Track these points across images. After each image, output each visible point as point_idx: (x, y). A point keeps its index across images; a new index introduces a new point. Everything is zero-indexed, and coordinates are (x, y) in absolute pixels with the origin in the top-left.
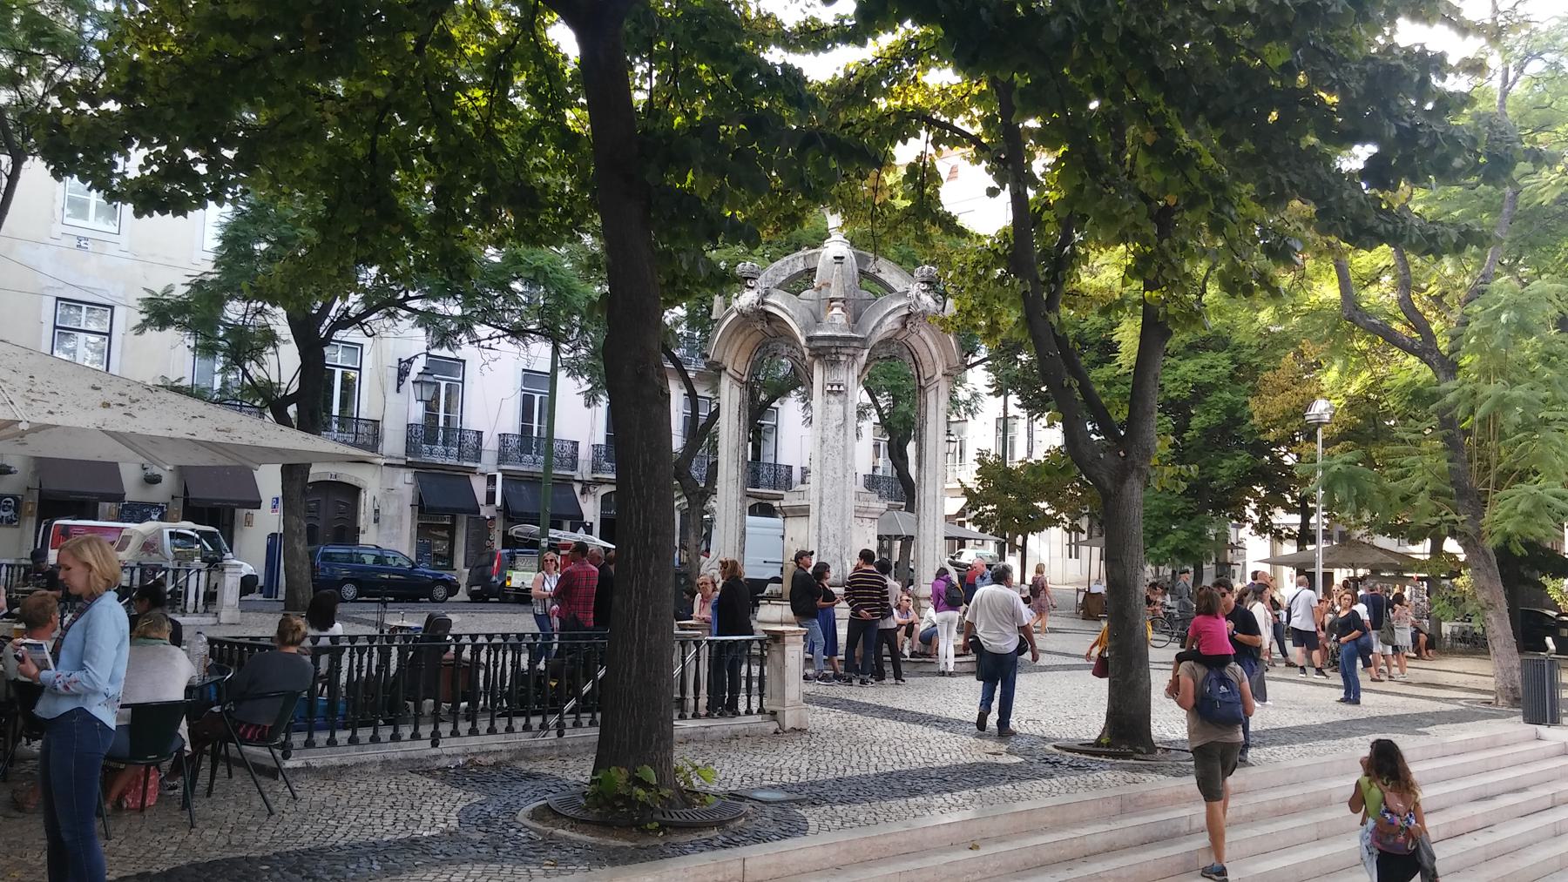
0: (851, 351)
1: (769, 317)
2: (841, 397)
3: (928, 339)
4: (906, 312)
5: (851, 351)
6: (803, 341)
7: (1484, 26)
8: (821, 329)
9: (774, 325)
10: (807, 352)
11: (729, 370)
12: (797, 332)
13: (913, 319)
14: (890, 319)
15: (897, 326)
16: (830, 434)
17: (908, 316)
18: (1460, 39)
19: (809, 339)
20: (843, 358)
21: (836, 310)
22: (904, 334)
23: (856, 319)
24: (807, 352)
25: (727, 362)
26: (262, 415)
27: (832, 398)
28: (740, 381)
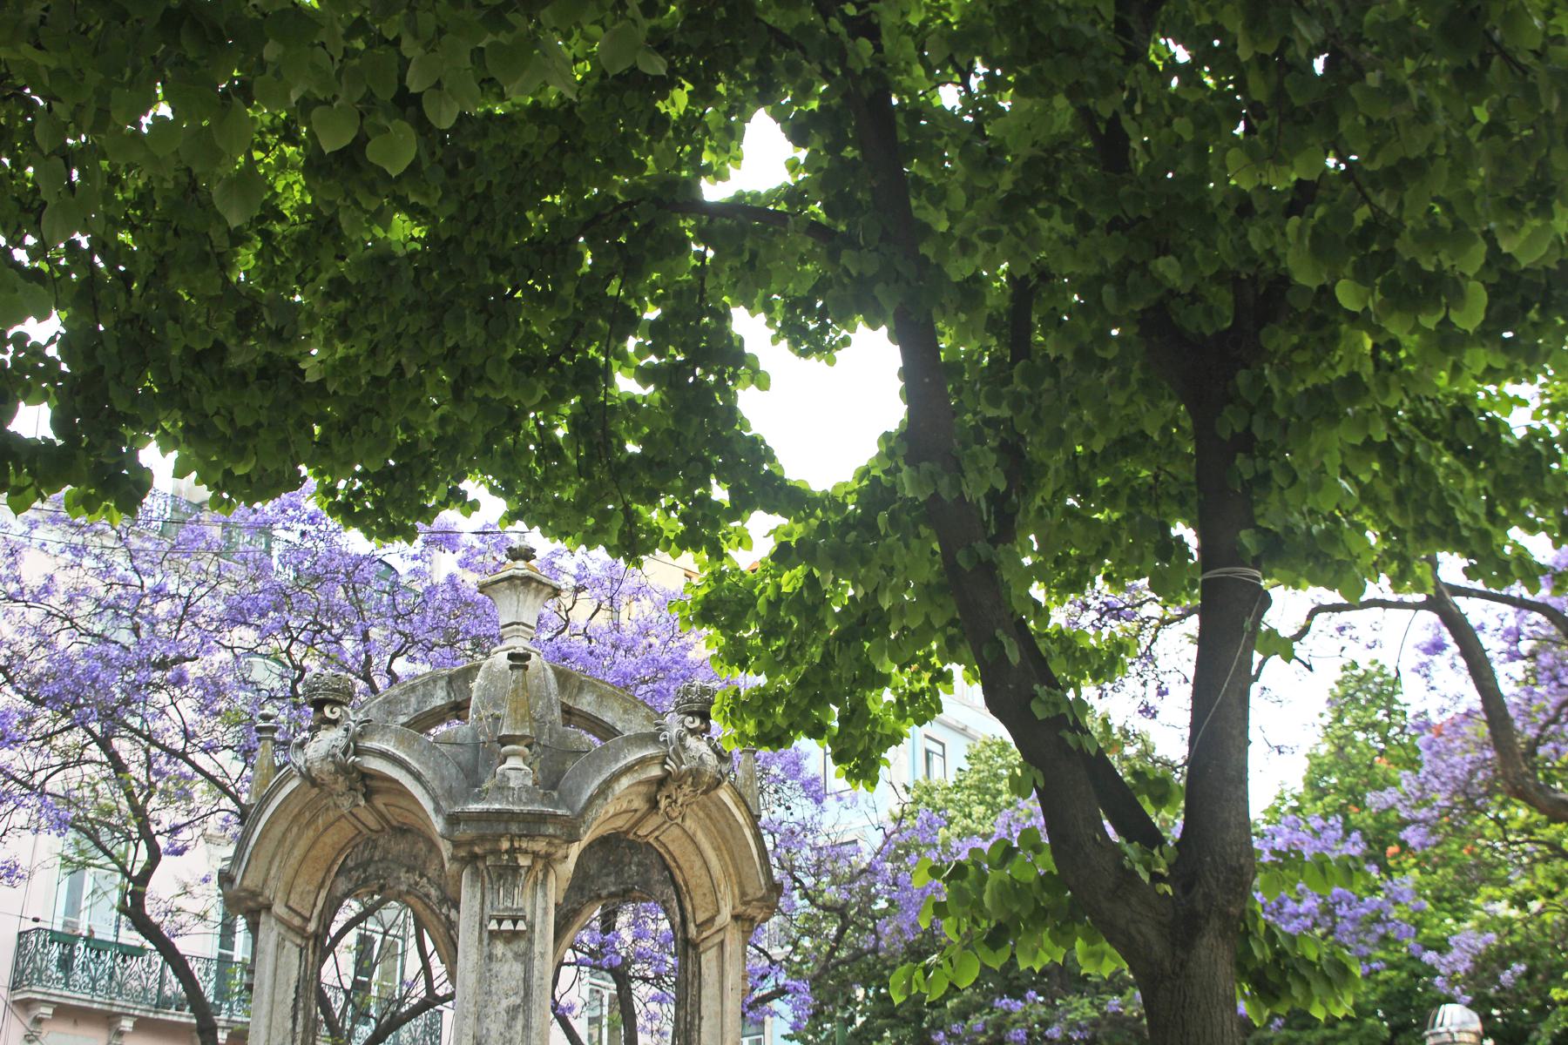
0: (540, 846)
1: (367, 784)
2: (521, 945)
3: (701, 838)
4: (655, 771)
5: (540, 846)
6: (438, 824)
7: (838, 349)
8: (478, 798)
9: (379, 802)
10: (446, 849)
11: (279, 909)
12: (428, 806)
13: (671, 788)
14: (625, 782)
15: (639, 804)
16: (495, 1027)
17: (661, 782)
18: (814, 364)
19: (453, 820)
20: (524, 861)
21: (512, 762)
22: (654, 821)
23: (551, 780)
24: (446, 849)
25: (274, 892)
26: (122, 489)
27: (500, 948)
28: (300, 931)
